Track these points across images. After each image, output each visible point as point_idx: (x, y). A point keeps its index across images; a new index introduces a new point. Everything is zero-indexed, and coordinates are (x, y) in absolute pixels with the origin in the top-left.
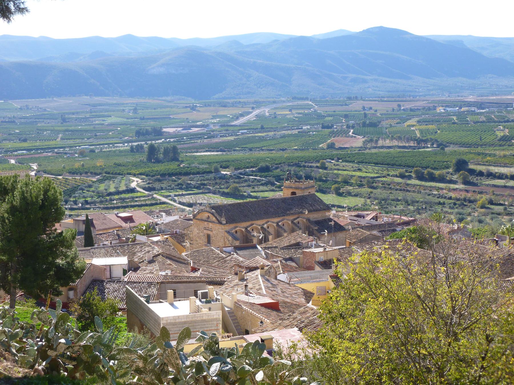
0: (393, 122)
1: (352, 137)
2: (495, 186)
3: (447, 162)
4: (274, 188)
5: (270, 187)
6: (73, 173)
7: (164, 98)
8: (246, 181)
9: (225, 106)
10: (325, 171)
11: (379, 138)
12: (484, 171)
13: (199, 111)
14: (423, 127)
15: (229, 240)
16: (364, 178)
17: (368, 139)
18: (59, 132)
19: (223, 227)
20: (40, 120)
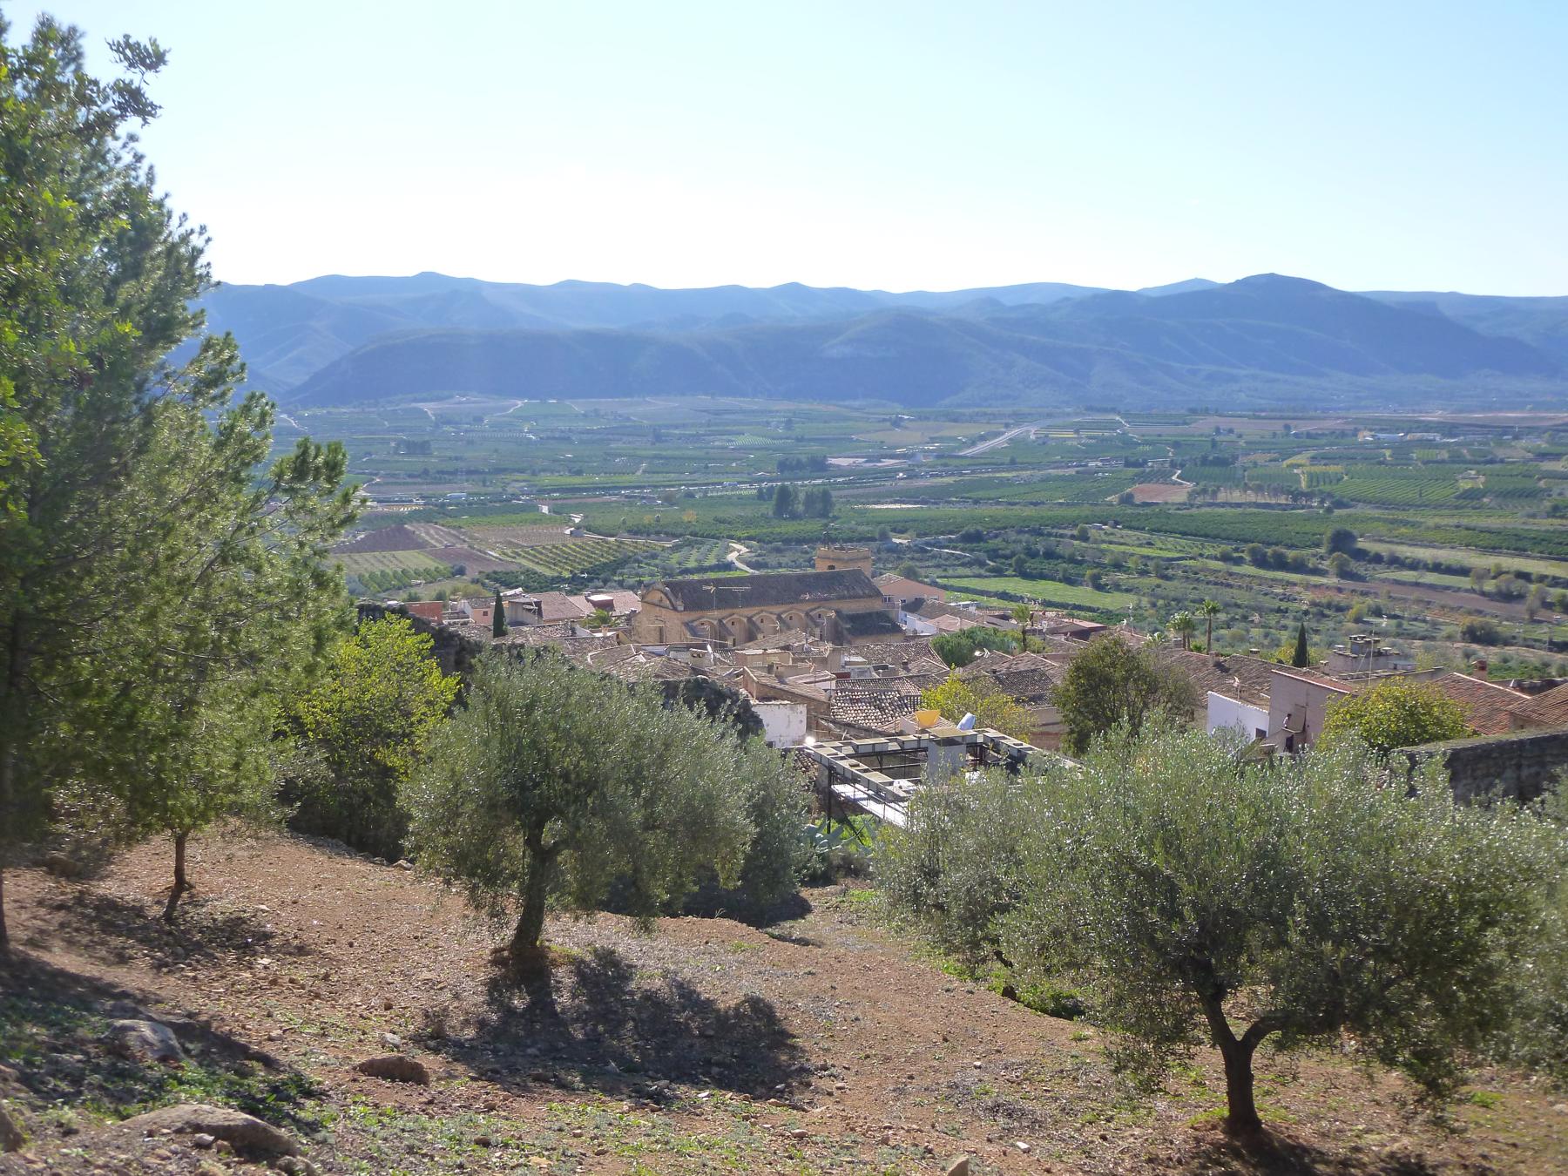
0: (1260, 458)
1: (1175, 483)
2: (1397, 582)
4: (982, 572)
5: (976, 569)
6: (636, 533)
7: (847, 403)
8: (934, 557)
9: (955, 421)
10: (1084, 544)
11: (1218, 488)
13: (906, 428)
14: (1319, 469)
16: (1152, 559)
17: (1198, 488)
18: (642, 459)
19: (679, 615)
20: (616, 437)
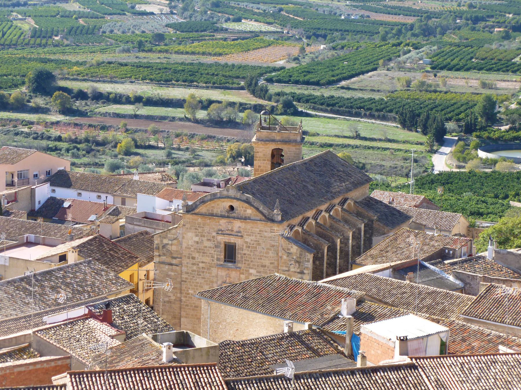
3: (6, 76)
12: (86, 91)
15: (289, 254)
19: (275, 227)
